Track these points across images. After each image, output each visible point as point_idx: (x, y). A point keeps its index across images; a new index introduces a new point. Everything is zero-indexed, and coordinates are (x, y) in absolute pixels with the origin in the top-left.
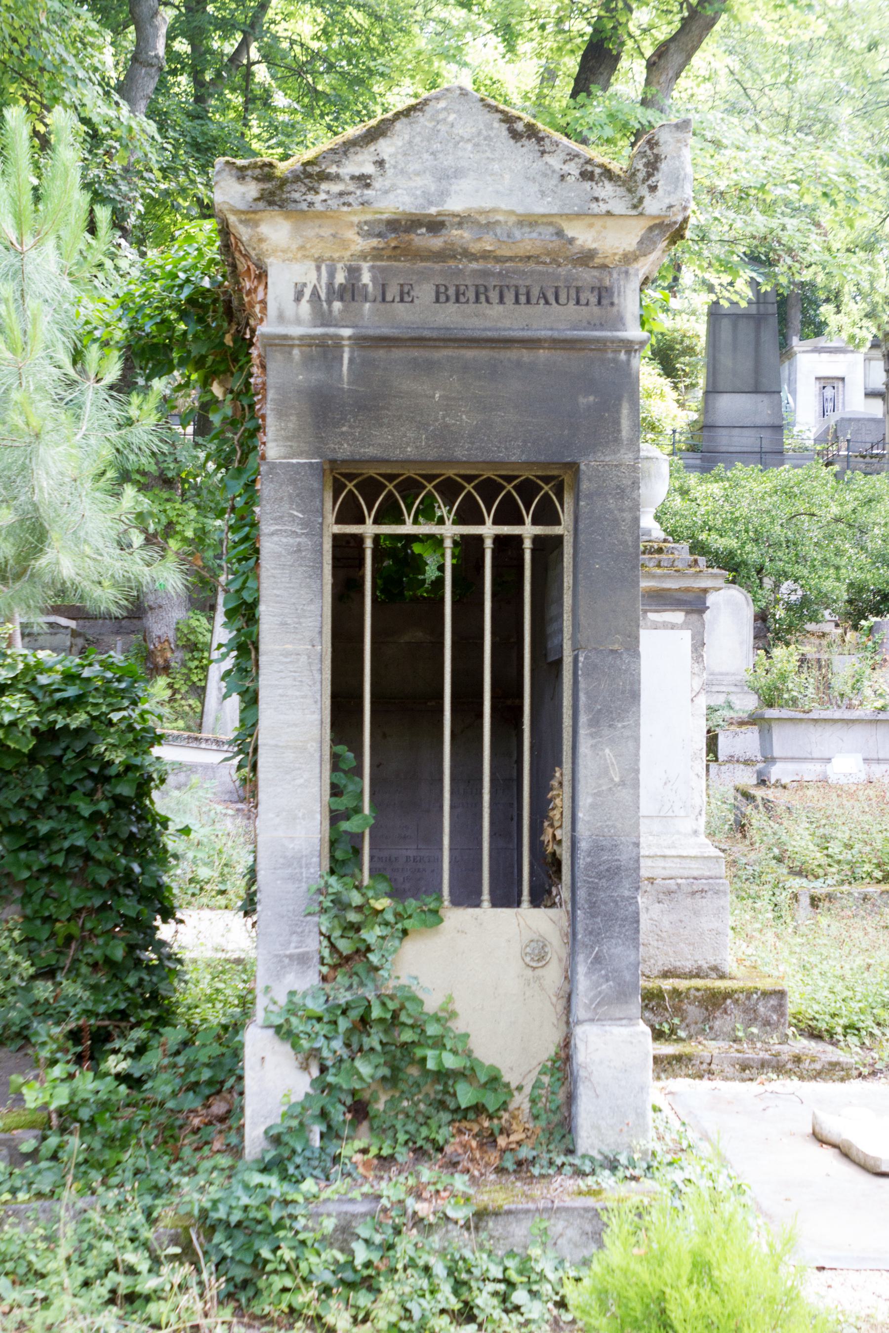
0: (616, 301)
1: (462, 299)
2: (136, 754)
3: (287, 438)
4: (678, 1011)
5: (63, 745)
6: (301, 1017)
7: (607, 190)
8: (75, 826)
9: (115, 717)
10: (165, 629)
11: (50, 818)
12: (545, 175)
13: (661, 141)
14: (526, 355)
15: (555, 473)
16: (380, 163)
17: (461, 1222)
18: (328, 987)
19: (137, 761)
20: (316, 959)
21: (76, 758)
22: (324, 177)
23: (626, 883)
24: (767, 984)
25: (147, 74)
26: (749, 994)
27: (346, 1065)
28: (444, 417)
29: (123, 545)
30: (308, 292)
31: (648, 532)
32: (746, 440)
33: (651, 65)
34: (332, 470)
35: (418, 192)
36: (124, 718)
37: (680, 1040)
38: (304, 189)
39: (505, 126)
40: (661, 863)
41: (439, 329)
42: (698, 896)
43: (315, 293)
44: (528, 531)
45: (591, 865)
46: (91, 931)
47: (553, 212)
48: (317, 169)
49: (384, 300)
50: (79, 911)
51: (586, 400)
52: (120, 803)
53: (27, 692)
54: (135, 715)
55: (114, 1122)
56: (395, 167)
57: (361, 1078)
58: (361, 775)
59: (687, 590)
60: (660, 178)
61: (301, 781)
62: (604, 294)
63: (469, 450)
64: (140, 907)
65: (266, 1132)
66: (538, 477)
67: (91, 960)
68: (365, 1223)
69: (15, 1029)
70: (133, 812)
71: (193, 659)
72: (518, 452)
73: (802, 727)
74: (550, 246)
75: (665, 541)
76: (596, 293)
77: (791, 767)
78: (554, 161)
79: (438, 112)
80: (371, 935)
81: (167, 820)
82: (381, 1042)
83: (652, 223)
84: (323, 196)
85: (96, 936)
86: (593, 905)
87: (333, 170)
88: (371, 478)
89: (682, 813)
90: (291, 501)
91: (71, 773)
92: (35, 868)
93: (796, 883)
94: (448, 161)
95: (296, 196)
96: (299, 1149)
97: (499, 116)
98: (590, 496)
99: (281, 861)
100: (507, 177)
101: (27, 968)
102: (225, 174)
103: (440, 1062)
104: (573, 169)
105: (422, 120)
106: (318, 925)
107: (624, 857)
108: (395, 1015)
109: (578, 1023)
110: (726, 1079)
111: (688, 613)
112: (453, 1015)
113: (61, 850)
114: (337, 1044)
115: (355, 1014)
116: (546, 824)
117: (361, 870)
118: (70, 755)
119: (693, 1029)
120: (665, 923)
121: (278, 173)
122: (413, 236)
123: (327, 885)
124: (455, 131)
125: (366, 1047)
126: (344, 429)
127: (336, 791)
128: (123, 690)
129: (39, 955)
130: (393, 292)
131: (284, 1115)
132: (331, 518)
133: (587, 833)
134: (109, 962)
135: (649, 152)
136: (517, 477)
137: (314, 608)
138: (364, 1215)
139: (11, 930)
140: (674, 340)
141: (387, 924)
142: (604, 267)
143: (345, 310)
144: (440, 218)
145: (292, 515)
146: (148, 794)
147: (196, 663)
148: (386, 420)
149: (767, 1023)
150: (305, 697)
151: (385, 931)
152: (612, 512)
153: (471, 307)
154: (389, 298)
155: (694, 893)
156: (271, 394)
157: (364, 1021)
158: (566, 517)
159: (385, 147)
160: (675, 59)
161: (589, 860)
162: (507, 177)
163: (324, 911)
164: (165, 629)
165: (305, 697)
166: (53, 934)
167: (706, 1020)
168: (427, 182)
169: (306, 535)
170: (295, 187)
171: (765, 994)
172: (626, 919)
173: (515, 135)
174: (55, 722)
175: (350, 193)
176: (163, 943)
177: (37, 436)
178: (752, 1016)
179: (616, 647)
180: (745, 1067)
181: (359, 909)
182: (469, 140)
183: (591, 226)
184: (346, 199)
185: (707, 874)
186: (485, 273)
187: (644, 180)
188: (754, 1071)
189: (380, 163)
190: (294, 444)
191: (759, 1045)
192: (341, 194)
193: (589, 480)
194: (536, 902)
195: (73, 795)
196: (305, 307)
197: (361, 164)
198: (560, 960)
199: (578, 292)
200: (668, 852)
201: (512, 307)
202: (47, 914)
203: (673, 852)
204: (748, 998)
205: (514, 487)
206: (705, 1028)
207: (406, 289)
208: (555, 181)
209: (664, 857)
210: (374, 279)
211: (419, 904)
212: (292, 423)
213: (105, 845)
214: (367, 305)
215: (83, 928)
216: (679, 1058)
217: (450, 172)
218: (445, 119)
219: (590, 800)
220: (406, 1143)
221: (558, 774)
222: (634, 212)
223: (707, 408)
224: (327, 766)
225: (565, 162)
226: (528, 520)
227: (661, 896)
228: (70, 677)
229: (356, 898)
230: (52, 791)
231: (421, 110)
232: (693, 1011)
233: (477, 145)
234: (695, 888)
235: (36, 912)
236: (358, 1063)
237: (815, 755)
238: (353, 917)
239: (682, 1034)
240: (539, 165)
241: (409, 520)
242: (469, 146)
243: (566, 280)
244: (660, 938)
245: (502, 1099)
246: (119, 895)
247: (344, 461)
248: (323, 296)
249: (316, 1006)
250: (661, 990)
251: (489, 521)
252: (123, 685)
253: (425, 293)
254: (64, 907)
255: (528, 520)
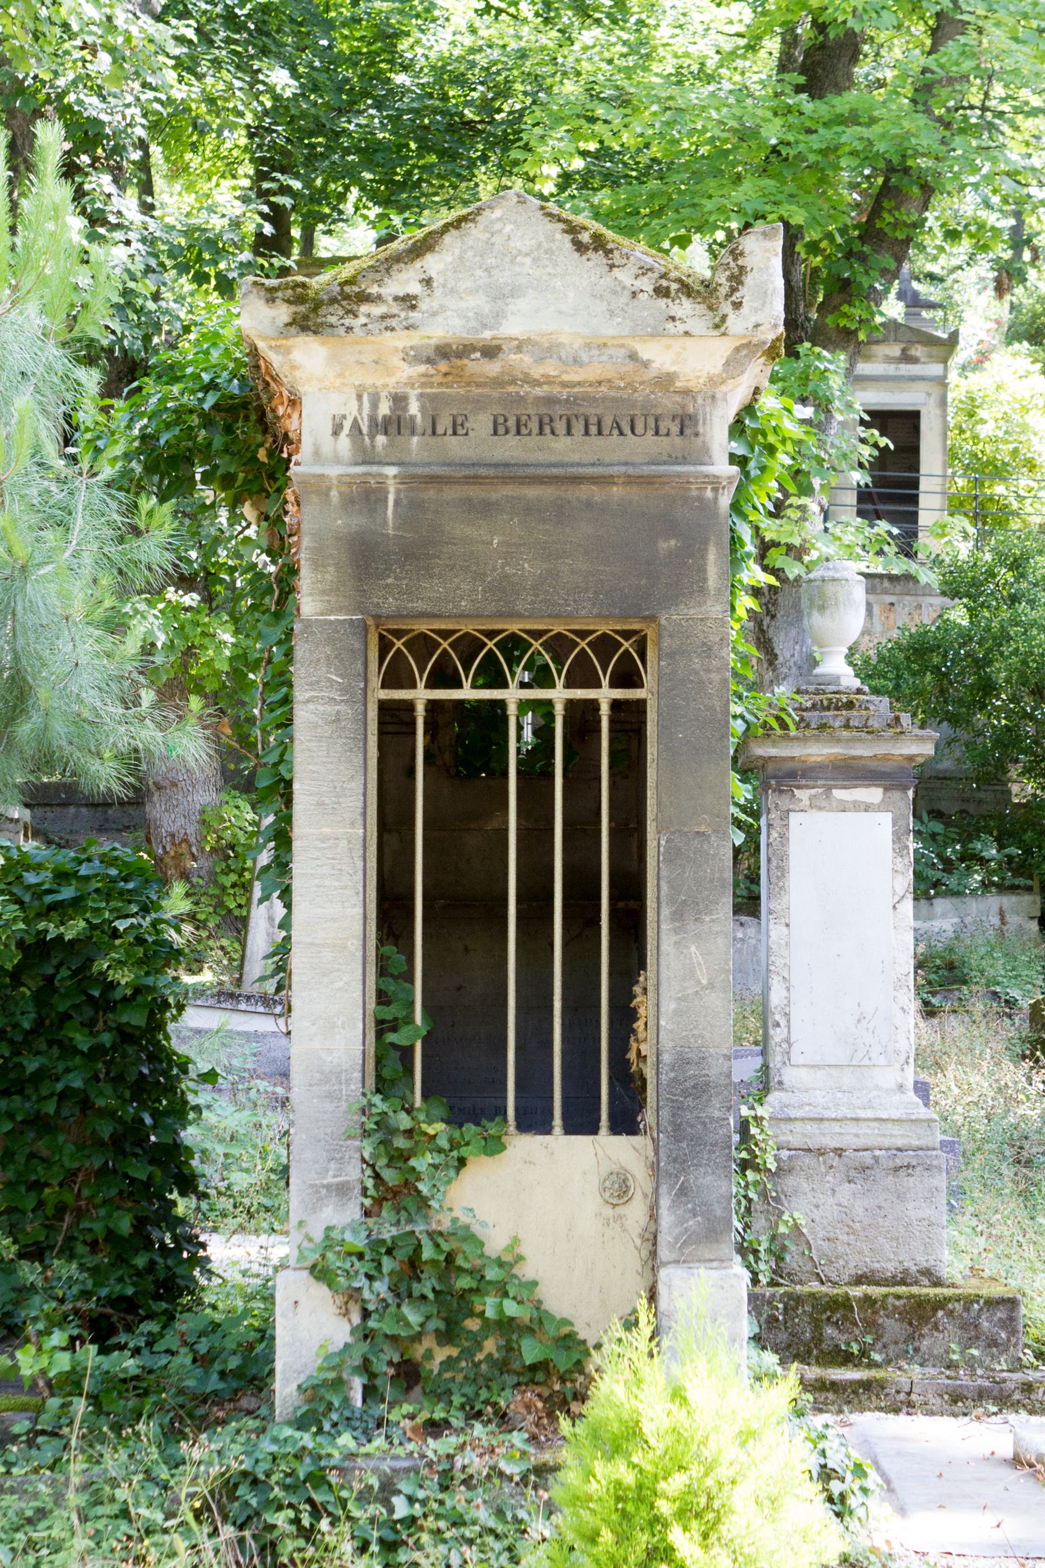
0: (701, 430)
1: (524, 431)
2: (147, 974)
3: (324, 592)
4: (871, 1325)
5: (55, 962)
6: (339, 1253)
7: (684, 307)
8: (70, 1064)
9: (122, 925)
11: (38, 1053)
12: (614, 292)
13: (747, 251)
14: (595, 493)
15: (636, 627)
16: (428, 282)
17: (517, 1478)
18: (370, 1221)
19: (150, 981)
20: (358, 1190)
21: (71, 977)
22: (364, 298)
23: (716, 1102)
24: (997, 1291)
26: (969, 1301)
27: (393, 1309)
28: (503, 566)
29: (130, 701)
30: (347, 425)
34: (377, 627)
35: (471, 314)
36: (132, 925)
37: (872, 1365)
38: (341, 313)
39: (568, 238)
40: (852, 1128)
41: (496, 465)
42: (902, 1173)
43: (356, 425)
44: (605, 695)
46: (90, 1199)
47: (623, 334)
48: (356, 289)
49: (434, 433)
50: (74, 1174)
51: (667, 545)
52: (126, 1035)
53: (11, 894)
54: (146, 922)
55: (122, 1402)
56: (444, 286)
57: (408, 1324)
58: (411, 980)
59: (886, 757)
60: (745, 292)
61: (341, 984)
62: (687, 422)
63: (532, 603)
64: (151, 1168)
65: (299, 1387)
66: (616, 632)
67: (89, 1238)
68: (408, 1478)
72: (588, 605)
74: (624, 369)
75: (859, 691)
76: (678, 421)
78: (625, 276)
79: (492, 222)
80: (422, 1163)
82: (434, 1290)
83: (738, 344)
84: (363, 320)
85: (95, 1207)
86: (677, 1127)
87: (374, 290)
89: (882, 1060)
90: (329, 665)
91: (65, 996)
92: (19, 1118)
94: (503, 278)
95: (332, 320)
96: (336, 1404)
97: (561, 226)
98: (671, 655)
99: (317, 1076)
100: (571, 295)
102: (252, 296)
103: (501, 1310)
104: (646, 284)
105: (474, 232)
106: (360, 1150)
108: (450, 1258)
109: (665, 1264)
111: (886, 789)
112: (520, 1258)
113: (52, 1094)
114: (381, 1287)
115: (402, 1254)
116: (632, 1039)
117: (413, 1092)
118: (64, 973)
119: (892, 1350)
121: (311, 293)
122: (465, 361)
123: (371, 1105)
124: (512, 244)
125: (416, 1294)
126: (389, 581)
127: (383, 998)
128: (129, 891)
129: (23, 1230)
130: (444, 424)
131: (321, 1369)
132: (376, 681)
133: (671, 1044)
134: (111, 1235)
135: (732, 264)
136: (594, 631)
138: (407, 1470)
141: (440, 1151)
142: (686, 392)
143: (391, 445)
144: (495, 342)
145: (329, 680)
146: (161, 1026)
147: (233, 877)
148: (436, 571)
150: (345, 887)
151: (438, 1159)
152: (697, 673)
153: (534, 440)
154: (440, 430)
155: (897, 1169)
156: (306, 542)
157: (414, 1265)
158: (649, 679)
159: (432, 263)
161: (672, 1075)
162: (571, 295)
165: (345, 887)
166: (41, 1204)
167: (910, 1338)
168: (480, 302)
169: (346, 702)
170: (331, 309)
171: (992, 1303)
172: (715, 1145)
173: (580, 247)
174: (47, 931)
175: (394, 316)
176: (182, 1221)
177: (24, 568)
178: (971, 1333)
179: (702, 829)
180: (956, 1398)
181: (409, 1133)
182: (527, 255)
183: (668, 347)
184: (391, 322)
187: (727, 296)
188: (971, 1403)
189: (428, 282)
190: (333, 599)
191: (979, 1372)
192: (383, 317)
193: (671, 636)
194: (616, 1129)
195: (68, 1024)
196: (344, 442)
197: (408, 281)
198: (645, 1196)
199: (656, 420)
200: (862, 1114)
201: (581, 439)
202: (34, 1178)
203: (870, 1114)
204: (967, 1309)
205: (588, 644)
207: (459, 420)
209: (857, 1119)
210: (423, 409)
211: (479, 1129)
212: (330, 574)
213: (108, 1089)
214: (415, 439)
215: (78, 1196)
216: (867, 1385)
217: (507, 291)
218: (500, 231)
219: (673, 1006)
220: (462, 1407)
221: (642, 979)
222: (716, 333)
224: (372, 970)
225: (637, 277)
226: (605, 682)
227: (853, 1173)
229: (404, 1121)
230: (39, 1022)
231: (473, 221)
232: (893, 1327)
234: (898, 1162)
235: (19, 1174)
236: (406, 1310)
238: (400, 1142)
239: (877, 1357)
240: (607, 280)
242: (528, 261)
243: (643, 407)
244: (851, 1231)
245: (576, 1356)
246: (124, 1154)
247: (388, 617)
248: (365, 429)
249: (359, 1242)
250: (847, 1298)
251: (560, 683)
252: (131, 885)
253: (481, 424)
254: (55, 1169)
255: (605, 682)
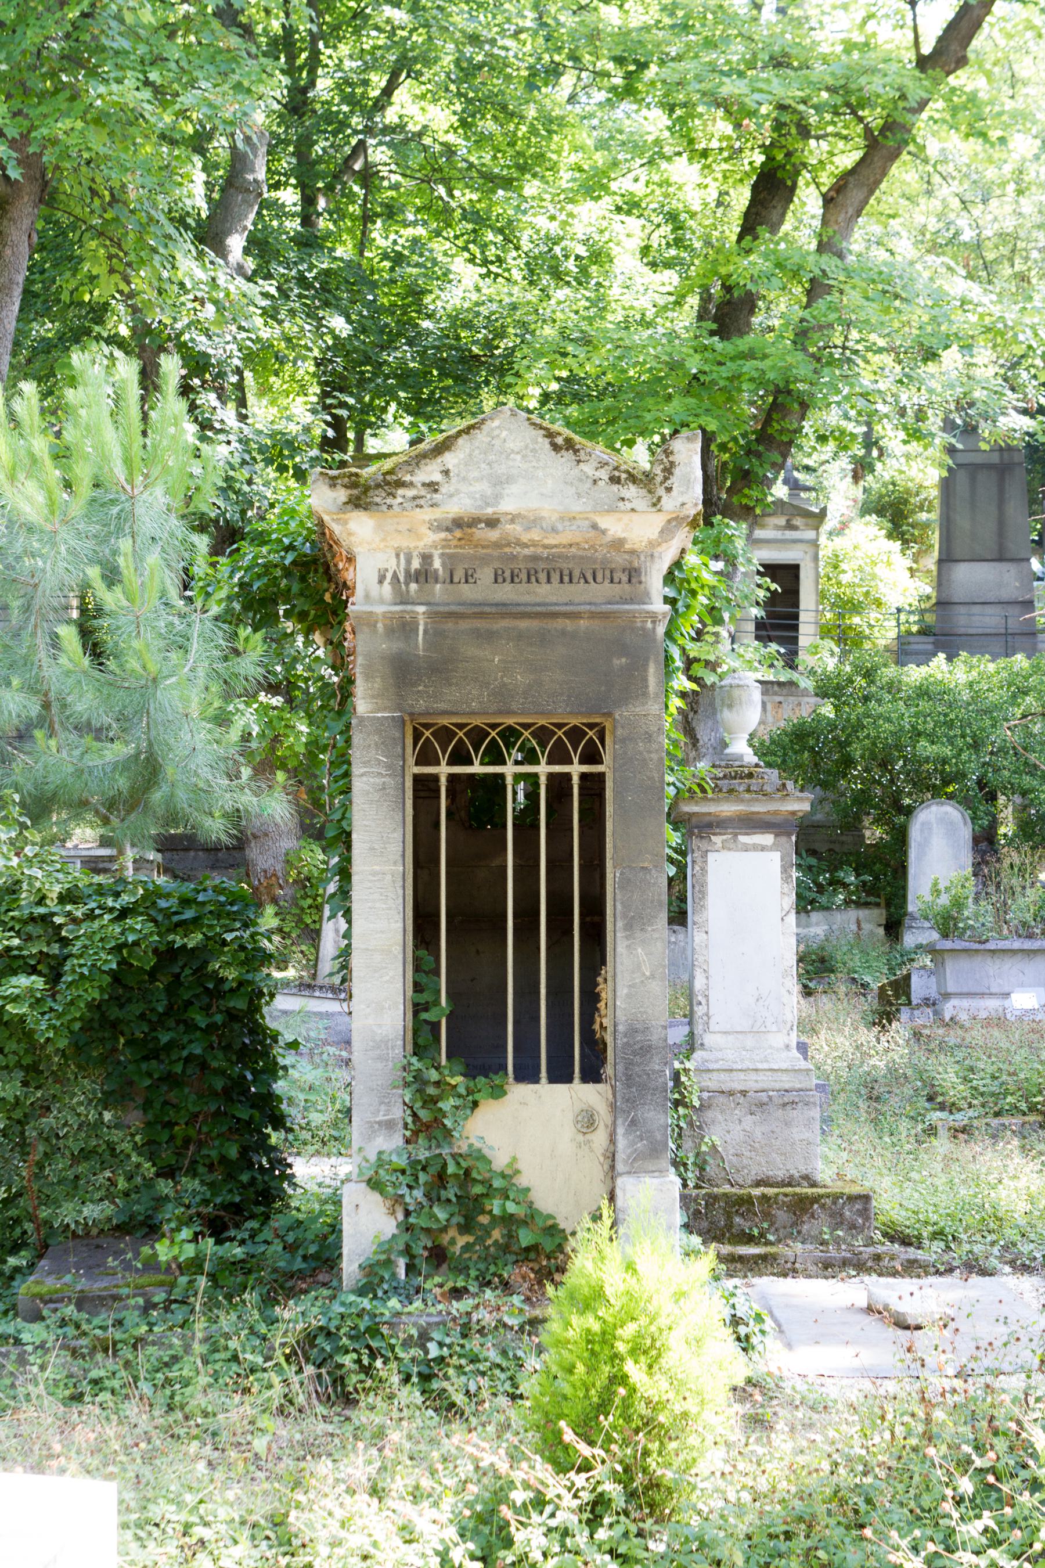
3: (373, 697)
4: (767, 1215)
9: (229, 937)
10: (271, 861)
14: (568, 624)
16: (446, 473)
19: (250, 977)
20: (401, 1125)
22: (400, 484)
24: (855, 1190)
25: (244, 201)
26: (836, 1197)
27: (426, 1209)
29: (233, 775)
30: (389, 576)
31: (740, 757)
32: (989, 619)
33: (828, 201)
37: (768, 1243)
40: (753, 1076)
41: (497, 605)
43: (395, 576)
44: (576, 769)
45: (627, 1044)
46: (207, 1134)
50: (196, 1116)
52: (232, 1016)
57: (438, 1220)
60: (675, 481)
69: (141, 1218)
70: (245, 1025)
71: (306, 896)
73: (978, 959)
75: (757, 766)
77: (965, 1003)
78: (588, 469)
81: (278, 1033)
84: (399, 500)
86: (629, 1078)
87: (407, 478)
88: (445, 727)
89: (774, 1028)
93: (936, 1116)
94: (501, 469)
95: (378, 500)
98: (623, 741)
101: (148, 1169)
103: (504, 1210)
104: (604, 474)
106: (402, 1096)
107: (655, 1037)
110: (810, 1277)
111: (776, 835)
112: (517, 1172)
115: (433, 1170)
118: (188, 971)
120: (758, 1134)
127: (418, 987)
130: (459, 575)
131: (376, 1253)
132: (411, 760)
134: (223, 1159)
137: (398, 835)
139: (133, 1135)
140: (908, 491)
141: (460, 1096)
142: (633, 552)
143: (420, 590)
147: (309, 901)
149: (853, 1226)
151: (458, 1102)
155: (784, 1105)
156: (360, 660)
157: (441, 1178)
158: (607, 758)
159: (449, 459)
160: (855, 195)
163: (407, 1085)
164: (271, 861)
167: (794, 1224)
168: (483, 487)
171: (852, 1199)
173: (556, 448)
177: (154, 680)
178: (838, 1220)
181: (437, 1084)
185: (798, 1086)
186: (535, 558)
189: (446, 473)
192: (414, 498)
196: (387, 588)
200: (760, 1066)
203: (765, 1066)
204: (834, 1203)
206: (794, 1232)
208: (589, 484)
210: (443, 564)
212: (378, 684)
213: (220, 1055)
215: (199, 1132)
216: (764, 1258)
223: (941, 581)
226: (576, 760)
228: (186, 902)
229: (434, 1075)
230: (170, 1007)
232: (782, 1216)
233: (524, 457)
237: (993, 990)
238: (431, 1091)
239: (771, 1238)
240: (576, 472)
241: (477, 762)
242: (518, 457)
244: (753, 1149)
245: (557, 1241)
246: (232, 1100)
249: (402, 1162)
250: (750, 1196)
255: (576, 760)
